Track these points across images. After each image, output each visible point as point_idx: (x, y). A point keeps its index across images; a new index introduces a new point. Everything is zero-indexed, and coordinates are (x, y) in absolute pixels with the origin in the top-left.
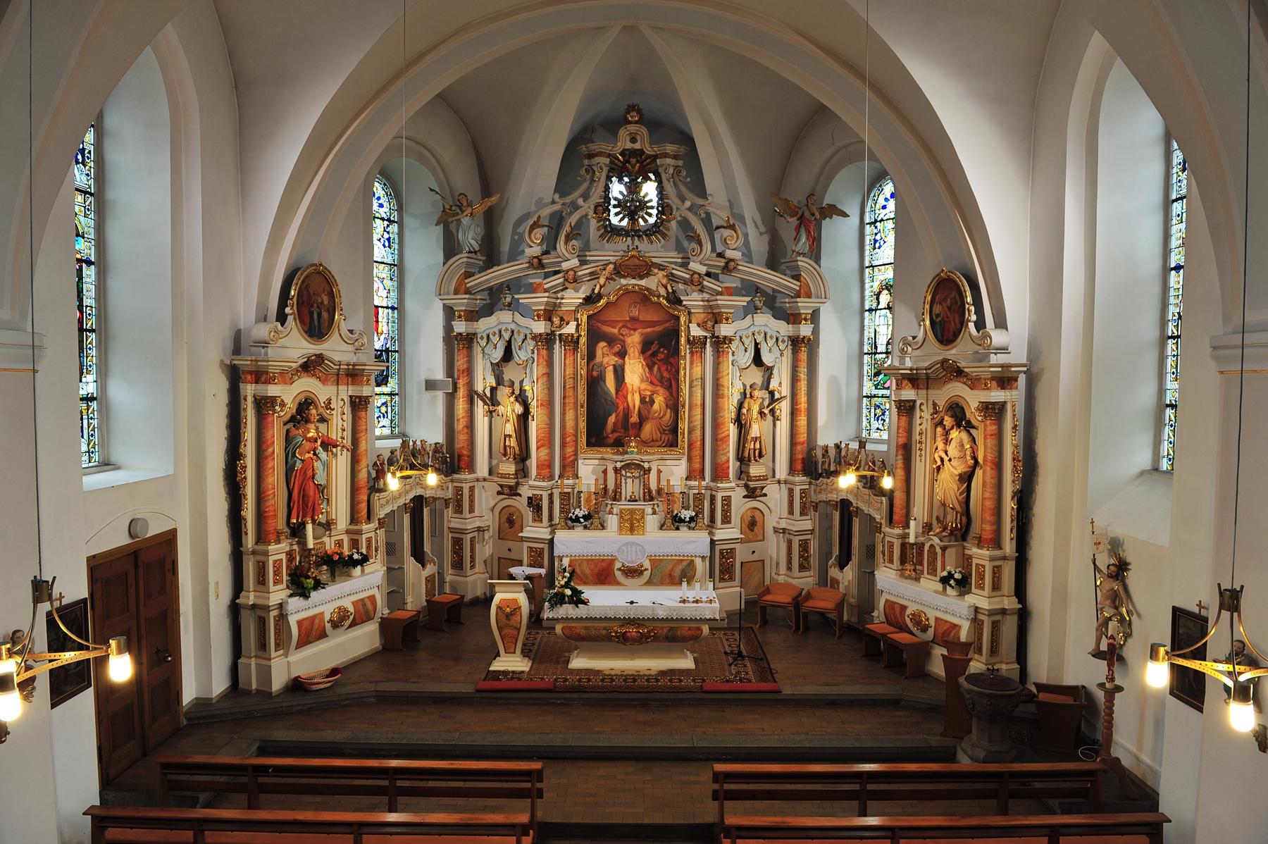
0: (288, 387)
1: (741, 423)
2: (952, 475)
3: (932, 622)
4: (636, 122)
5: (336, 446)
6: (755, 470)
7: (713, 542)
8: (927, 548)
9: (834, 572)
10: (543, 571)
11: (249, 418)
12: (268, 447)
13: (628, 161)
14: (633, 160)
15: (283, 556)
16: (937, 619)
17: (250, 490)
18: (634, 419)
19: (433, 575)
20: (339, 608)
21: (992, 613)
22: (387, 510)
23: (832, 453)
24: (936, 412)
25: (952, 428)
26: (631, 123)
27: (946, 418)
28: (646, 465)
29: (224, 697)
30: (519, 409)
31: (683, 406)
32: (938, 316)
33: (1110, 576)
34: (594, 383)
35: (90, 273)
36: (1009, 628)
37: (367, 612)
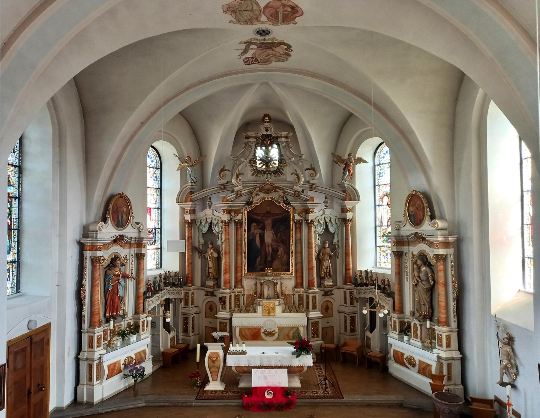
0: (106, 251)
1: (320, 261)
2: (423, 288)
3: (417, 363)
4: (268, 122)
5: (128, 278)
6: (328, 282)
7: (308, 319)
8: (412, 325)
9: (368, 334)
10: (227, 334)
11: (87, 267)
12: (96, 281)
13: (265, 140)
14: (267, 139)
15: (102, 333)
16: (420, 361)
17: (87, 302)
18: (269, 259)
19: (174, 337)
20: (128, 357)
21: (447, 359)
22: (153, 306)
23: (364, 275)
24: (413, 257)
25: (421, 266)
26: (265, 122)
27: (418, 261)
28: (275, 282)
29: (69, 406)
30: (215, 255)
31: (292, 253)
32: (412, 212)
33: (505, 344)
34: (250, 243)
35: (15, 203)
36: (457, 366)
37: (142, 358)
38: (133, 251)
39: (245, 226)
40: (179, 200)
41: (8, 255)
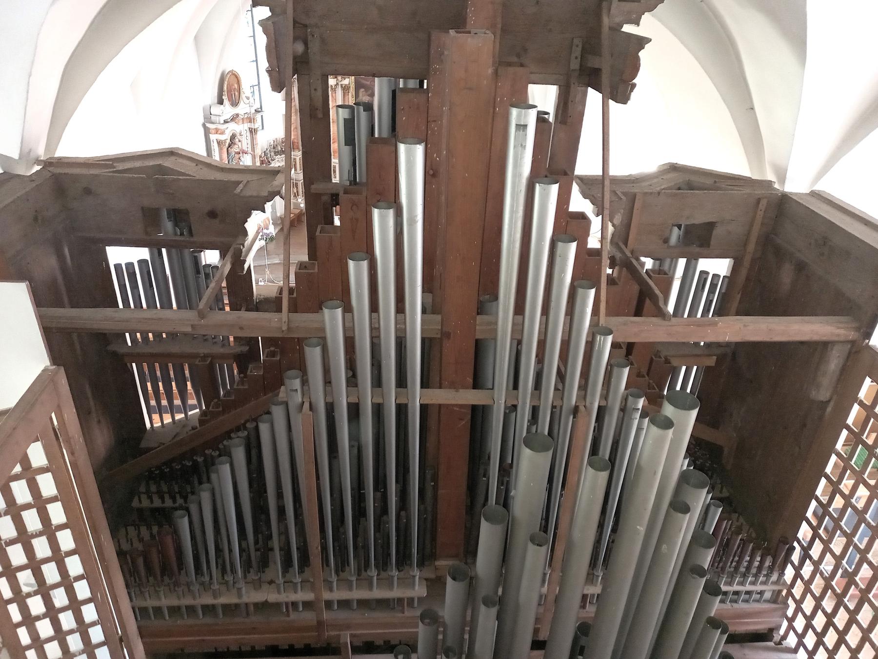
38: (246, 126)
39: (352, 91)
40: (278, 85)
41: (479, 317)
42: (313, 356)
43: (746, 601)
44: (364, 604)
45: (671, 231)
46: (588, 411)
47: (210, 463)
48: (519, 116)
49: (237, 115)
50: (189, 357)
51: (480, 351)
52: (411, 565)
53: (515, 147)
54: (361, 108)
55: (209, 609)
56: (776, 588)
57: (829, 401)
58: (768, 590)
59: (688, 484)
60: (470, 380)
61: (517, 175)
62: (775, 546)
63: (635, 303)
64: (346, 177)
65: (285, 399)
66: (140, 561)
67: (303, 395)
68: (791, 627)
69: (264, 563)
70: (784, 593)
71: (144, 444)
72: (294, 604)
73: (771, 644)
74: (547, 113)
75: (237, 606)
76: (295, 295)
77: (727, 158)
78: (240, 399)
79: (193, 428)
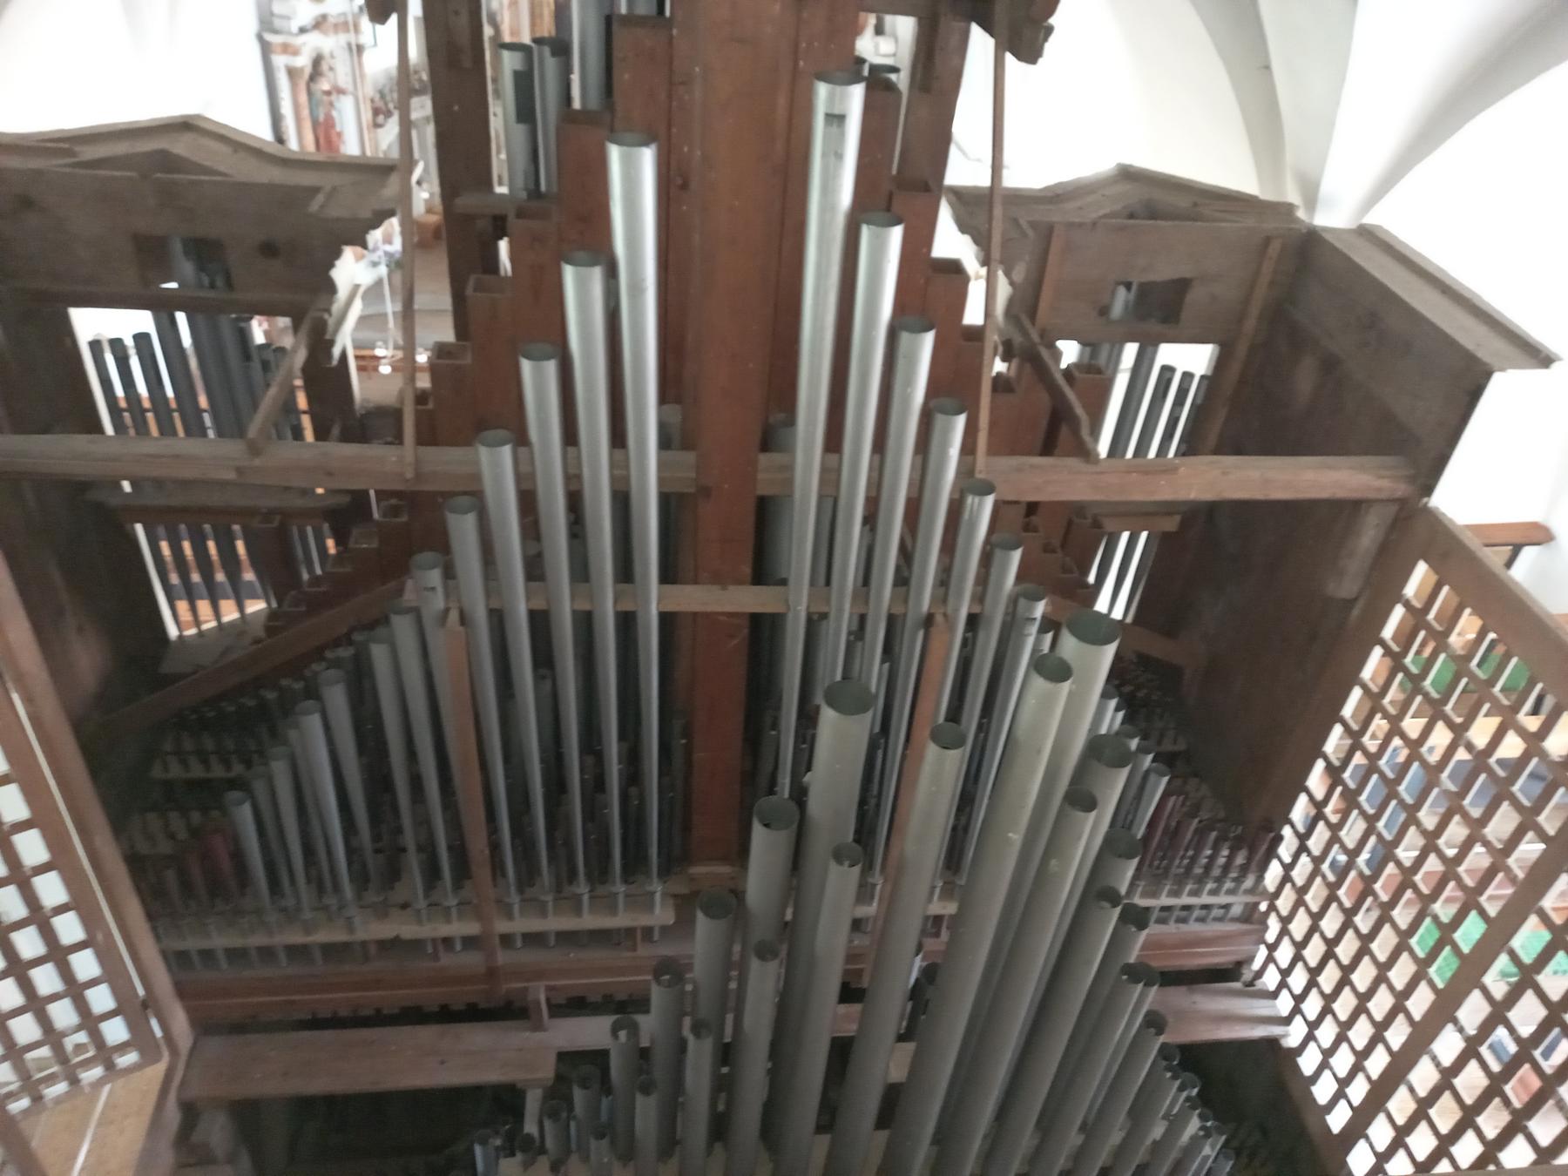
41: (764, 459)
42: (463, 528)
43: (1201, 920)
44: (568, 938)
45: (1113, 293)
46: (950, 621)
47: (289, 706)
48: (831, 98)
49: (324, 17)
50: (243, 514)
51: (766, 516)
52: (648, 874)
53: (824, 155)
54: (547, 50)
55: (298, 952)
56: (1250, 899)
57: (1356, 599)
58: (1238, 904)
59: (1099, 760)
60: (747, 570)
61: (828, 206)
62: (1255, 836)
63: (1044, 423)
64: (520, 182)
65: (414, 604)
66: (170, 876)
67: (447, 595)
68: (1270, 959)
69: (393, 874)
70: (1263, 907)
71: (167, 668)
72: (447, 942)
73: (1237, 985)
74: (895, 70)
75: (346, 946)
76: (430, 406)
77: (1215, 158)
78: (338, 588)
79: (257, 641)
